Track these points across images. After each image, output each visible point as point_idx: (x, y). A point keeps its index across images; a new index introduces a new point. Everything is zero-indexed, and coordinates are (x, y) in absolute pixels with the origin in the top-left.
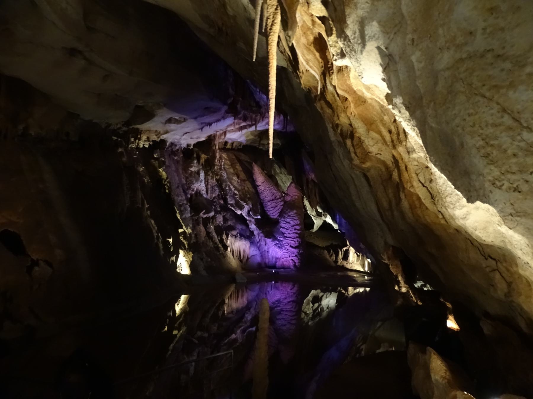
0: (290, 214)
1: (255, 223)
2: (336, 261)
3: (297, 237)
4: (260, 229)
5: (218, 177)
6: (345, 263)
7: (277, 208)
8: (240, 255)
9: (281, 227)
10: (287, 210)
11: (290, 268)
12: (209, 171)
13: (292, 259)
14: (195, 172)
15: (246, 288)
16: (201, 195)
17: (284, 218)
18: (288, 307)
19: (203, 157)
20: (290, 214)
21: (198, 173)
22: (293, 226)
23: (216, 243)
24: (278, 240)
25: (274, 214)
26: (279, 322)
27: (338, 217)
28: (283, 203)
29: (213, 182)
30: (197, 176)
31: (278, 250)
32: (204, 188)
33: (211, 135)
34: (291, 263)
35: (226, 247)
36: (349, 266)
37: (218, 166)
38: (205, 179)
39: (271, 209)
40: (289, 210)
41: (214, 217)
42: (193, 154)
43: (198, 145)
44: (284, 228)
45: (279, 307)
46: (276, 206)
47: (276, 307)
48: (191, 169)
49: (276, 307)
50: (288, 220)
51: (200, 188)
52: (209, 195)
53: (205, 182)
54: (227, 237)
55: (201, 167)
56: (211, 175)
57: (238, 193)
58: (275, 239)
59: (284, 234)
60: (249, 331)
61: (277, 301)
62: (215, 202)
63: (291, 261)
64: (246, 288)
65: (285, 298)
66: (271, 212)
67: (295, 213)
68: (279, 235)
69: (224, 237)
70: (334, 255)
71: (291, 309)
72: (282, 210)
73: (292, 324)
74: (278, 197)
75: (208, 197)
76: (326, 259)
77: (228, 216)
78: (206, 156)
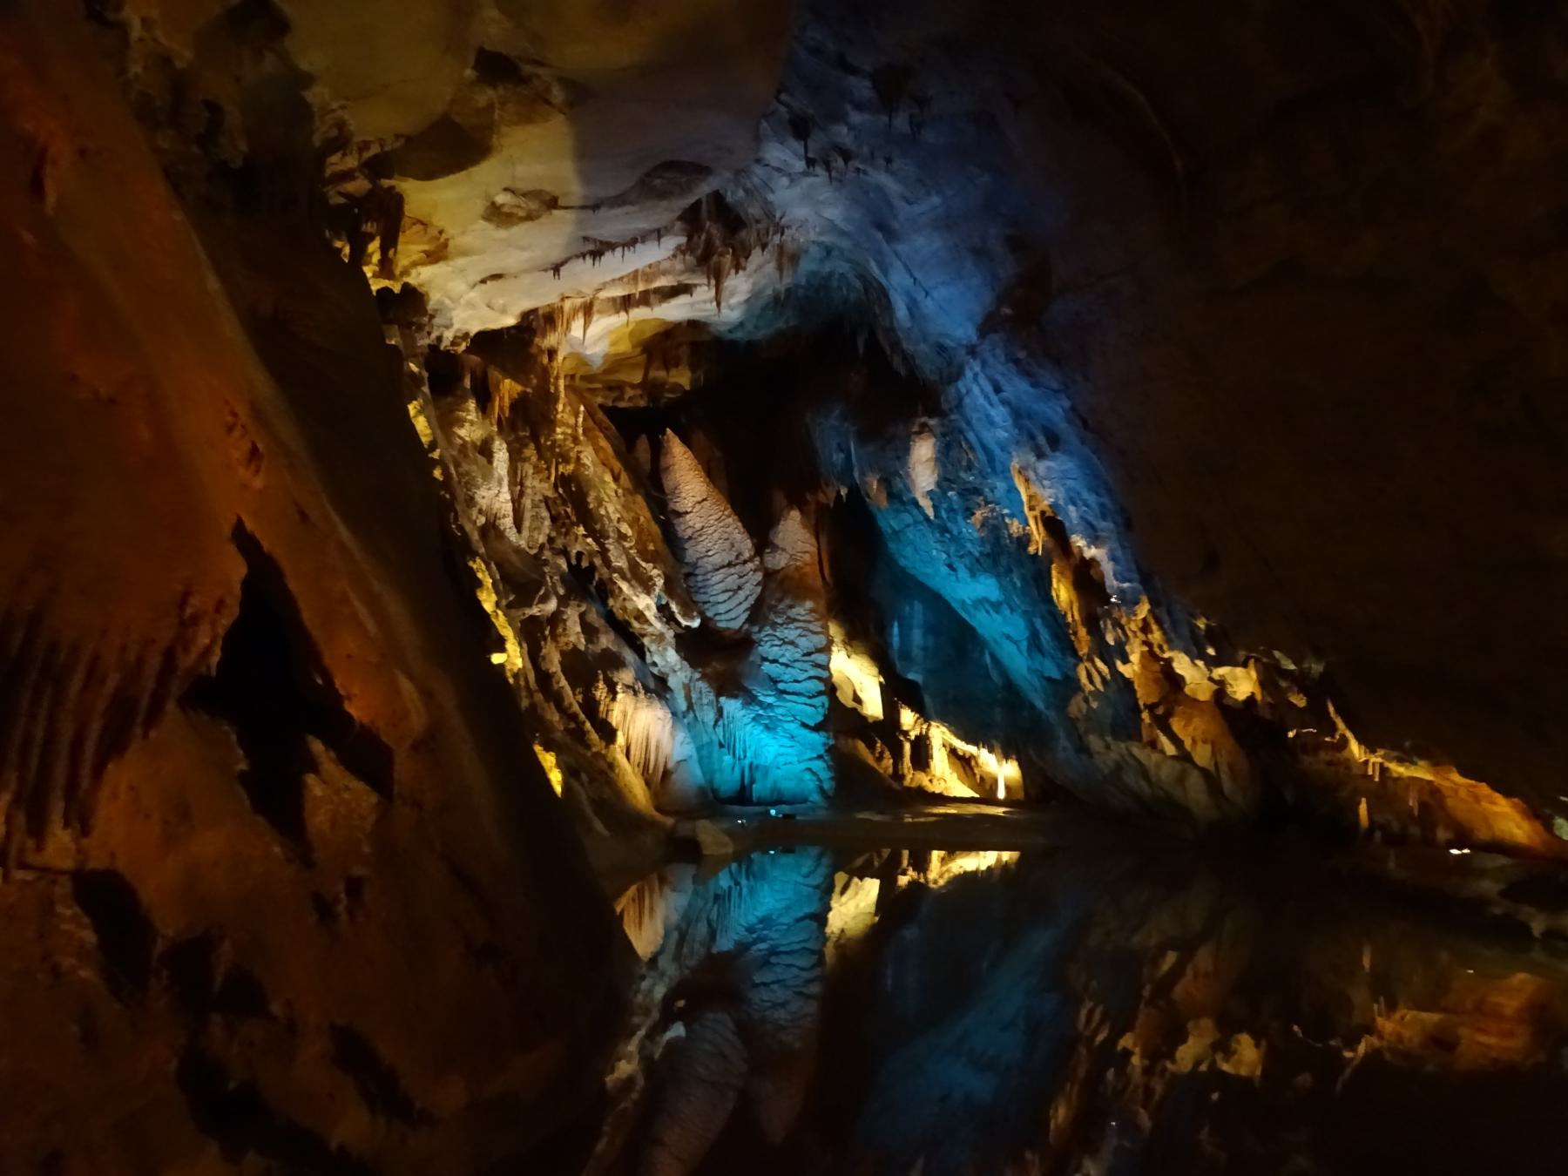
0: (793, 613)
1: (673, 641)
2: (898, 776)
3: (820, 693)
4: (694, 664)
5: (571, 467)
6: (922, 779)
7: (742, 594)
9: (765, 659)
10: (781, 600)
11: (805, 801)
12: (526, 446)
13: (809, 769)
14: (473, 443)
16: (501, 535)
17: (774, 625)
19: (508, 388)
21: (485, 450)
22: (809, 654)
23: (574, 717)
24: (761, 704)
28: (759, 576)
29: (539, 487)
30: (482, 460)
31: (766, 737)
33: (534, 311)
36: (936, 788)
37: (567, 425)
38: (513, 471)
40: (788, 601)
41: (556, 619)
42: (461, 379)
44: (775, 661)
45: (763, 940)
46: (740, 588)
47: (755, 942)
49: (755, 942)
51: (497, 506)
52: (525, 533)
53: (512, 484)
54: (613, 692)
55: (495, 428)
56: (534, 459)
57: (630, 533)
58: (750, 700)
59: (775, 681)
60: (668, 1042)
61: (761, 921)
62: (546, 563)
63: (807, 776)
65: (788, 908)
66: (722, 608)
67: (812, 611)
68: (761, 686)
69: (601, 692)
70: (887, 754)
72: (760, 601)
73: (809, 997)
74: (747, 555)
75: (523, 544)
76: (873, 769)
77: (594, 618)
78: (519, 388)
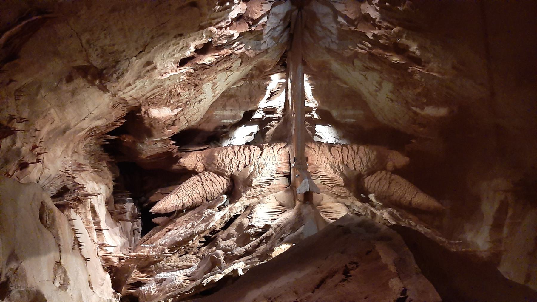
0: (220, 160)
2: (279, 119)
3: (249, 149)
7: (213, 179)
8: (277, 212)
15: (319, 205)
18: (338, 155)
19: (135, 275)
20: (220, 160)
21: (160, 282)
23: (261, 241)
25: (221, 183)
26: (359, 167)
27: (225, 121)
28: (206, 173)
29: (174, 260)
32: (183, 271)
34: (283, 152)
35: (267, 227)
37: (149, 250)
39: (215, 187)
40: (216, 162)
41: (225, 251)
43: (116, 285)
48: (153, 292)
49: (340, 170)
50: (228, 160)
52: (192, 264)
53: (173, 270)
62: (203, 255)
64: (319, 205)
68: (247, 171)
69: (251, 231)
70: (271, 123)
71: (340, 151)
74: (198, 178)
75: (196, 264)
78: (135, 270)
